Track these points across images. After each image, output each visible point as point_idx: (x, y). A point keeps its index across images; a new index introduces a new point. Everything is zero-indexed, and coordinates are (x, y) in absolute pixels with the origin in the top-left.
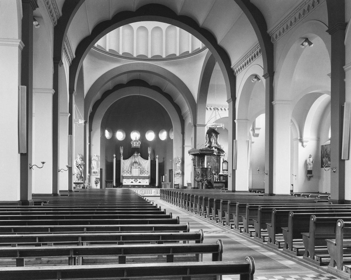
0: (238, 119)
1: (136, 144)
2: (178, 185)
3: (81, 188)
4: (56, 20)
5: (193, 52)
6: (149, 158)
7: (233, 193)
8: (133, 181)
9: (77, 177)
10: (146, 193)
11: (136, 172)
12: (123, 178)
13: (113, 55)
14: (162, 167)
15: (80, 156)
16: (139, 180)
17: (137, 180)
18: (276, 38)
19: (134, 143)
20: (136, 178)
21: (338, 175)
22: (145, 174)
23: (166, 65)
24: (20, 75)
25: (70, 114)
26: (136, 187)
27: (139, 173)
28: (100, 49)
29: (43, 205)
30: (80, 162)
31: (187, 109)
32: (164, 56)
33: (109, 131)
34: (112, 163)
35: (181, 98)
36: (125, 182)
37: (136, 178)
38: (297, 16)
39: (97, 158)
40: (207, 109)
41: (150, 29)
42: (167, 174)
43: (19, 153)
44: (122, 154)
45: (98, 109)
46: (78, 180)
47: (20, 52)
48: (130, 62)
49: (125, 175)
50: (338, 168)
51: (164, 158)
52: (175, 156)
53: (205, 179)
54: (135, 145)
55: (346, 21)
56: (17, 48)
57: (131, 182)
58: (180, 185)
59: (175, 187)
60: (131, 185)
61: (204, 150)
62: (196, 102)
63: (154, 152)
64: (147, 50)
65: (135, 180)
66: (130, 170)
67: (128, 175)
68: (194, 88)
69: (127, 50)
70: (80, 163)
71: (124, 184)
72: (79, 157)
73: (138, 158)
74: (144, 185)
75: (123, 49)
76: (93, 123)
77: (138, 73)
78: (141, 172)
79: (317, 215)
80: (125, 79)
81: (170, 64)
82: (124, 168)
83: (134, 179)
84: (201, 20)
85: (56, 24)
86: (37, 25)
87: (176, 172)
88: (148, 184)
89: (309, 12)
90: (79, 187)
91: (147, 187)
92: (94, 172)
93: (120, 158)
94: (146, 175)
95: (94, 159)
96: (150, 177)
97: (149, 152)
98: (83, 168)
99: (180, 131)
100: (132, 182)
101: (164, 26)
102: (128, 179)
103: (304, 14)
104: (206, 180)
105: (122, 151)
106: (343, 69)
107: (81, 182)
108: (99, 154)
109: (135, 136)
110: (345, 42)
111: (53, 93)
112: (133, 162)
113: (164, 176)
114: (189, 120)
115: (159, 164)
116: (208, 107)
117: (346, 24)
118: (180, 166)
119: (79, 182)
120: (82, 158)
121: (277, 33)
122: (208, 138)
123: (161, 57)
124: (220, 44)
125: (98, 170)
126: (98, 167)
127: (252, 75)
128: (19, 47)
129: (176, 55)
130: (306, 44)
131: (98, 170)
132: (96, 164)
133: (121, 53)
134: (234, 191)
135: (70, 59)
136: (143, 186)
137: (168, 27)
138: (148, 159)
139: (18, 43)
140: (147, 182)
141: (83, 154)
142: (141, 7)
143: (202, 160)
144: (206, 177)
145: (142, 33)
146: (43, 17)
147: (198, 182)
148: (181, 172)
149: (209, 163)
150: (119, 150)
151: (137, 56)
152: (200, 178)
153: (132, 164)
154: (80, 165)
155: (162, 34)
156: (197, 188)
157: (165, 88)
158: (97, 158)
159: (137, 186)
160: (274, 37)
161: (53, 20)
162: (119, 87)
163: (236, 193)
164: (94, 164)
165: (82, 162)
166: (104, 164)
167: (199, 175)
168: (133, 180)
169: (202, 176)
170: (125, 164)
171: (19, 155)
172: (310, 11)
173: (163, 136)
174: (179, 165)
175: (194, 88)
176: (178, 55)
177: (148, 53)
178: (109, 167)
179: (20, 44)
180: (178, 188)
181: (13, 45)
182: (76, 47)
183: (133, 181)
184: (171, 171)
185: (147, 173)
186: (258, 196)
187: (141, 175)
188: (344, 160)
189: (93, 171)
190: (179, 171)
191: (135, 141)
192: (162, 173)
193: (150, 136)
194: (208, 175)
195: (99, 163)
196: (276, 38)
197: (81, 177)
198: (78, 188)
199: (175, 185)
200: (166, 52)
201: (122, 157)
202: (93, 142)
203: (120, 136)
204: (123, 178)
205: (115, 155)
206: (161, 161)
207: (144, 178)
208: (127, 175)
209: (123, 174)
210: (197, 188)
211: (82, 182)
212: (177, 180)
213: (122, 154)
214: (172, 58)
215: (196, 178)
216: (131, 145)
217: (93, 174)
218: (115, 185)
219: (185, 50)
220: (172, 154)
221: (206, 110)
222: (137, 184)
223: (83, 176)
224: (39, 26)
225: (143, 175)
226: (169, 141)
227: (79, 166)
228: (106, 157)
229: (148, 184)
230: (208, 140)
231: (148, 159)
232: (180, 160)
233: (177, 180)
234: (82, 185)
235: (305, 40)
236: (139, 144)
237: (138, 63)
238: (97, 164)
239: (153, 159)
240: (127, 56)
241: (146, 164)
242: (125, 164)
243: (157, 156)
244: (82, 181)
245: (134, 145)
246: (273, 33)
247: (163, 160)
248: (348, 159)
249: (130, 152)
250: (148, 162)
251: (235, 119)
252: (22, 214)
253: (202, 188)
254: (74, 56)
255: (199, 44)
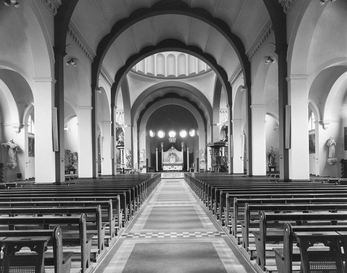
0: (234, 120)
1: (172, 140)
2: (203, 169)
3: (130, 173)
4: (92, 58)
5: (208, 70)
6: (182, 150)
7: (231, 175)
8: (171, 168)
9: (127, 165)
10: (178, 176)
11: (172, 161)
12: (164, 165)
13: (150, 77)
14: (192, 156)
15: (129, 150)
16: (175, 167)
17: (174, 167)
18: (251, 58)
19: (171, 139)
20: (172, 165)
21: (64, 162)
22: (180, 162)
23: (189, 81)
24: (54, 99)
25: (111, 122)
26: (172, 171)
27: (175, 161)
28: (140, 73)
29: (69, 185)
30: (128, 154)
31: (207, 114)
32: (187, 75)
33: (153, 131)
34: (155, 155)
35: (202, 105)
36: (165, 168)
37: (172, 165)
38: (261, 41)
39: (144, 151)
40: (221, 112)
41: (166, 56)
42: (195, 162)
43: (53, 151)
44: (162, 147)
45: (144, 117)
46: (128, 167)
47: (54, 85)
48: (161, 81)
49: (165, 163)
50: (283, 156)
51: (193, 150)
52: (200, 148)
53: (219, 165)
54: (171, 141)
55: (287, 43)
56: (50, 83)
57: (169, 168)
58: (204, 170)
59: (201, 171)
60: (169, 170)
61: (218, 143)
62: (212, 107)
63: (186, 146)
64: (175, 70)
65: (172, 167)
66: (168, 159)
67: (167, 163)
68: (211, 98)
69: (160, 72)
70: (128, 155)
71: (164, 169)
72: (127, 151)
73: (174, 151)
74: (167, 170)
75: (157, 71)
76: (140, 128)
77: (171, 89)
78: (177, 161)
79: (218, 188)
80: (161, 93)
81: (192, 80)
82: (164, 158)
83: (171, 166)
84: (203, 48)
85: (93, 61)
86: (75, 65)
87: (201, 160)
88: (181, 169)
89: (268, 37)
90: (128, 172)
91: (180, 171)
92: (141, 162)
93: (161, 150)
94: (180, 163)
95: (142, 152)
96: (183, 164)
97: (182, 146)
98: (131, 159)
99: (203, 129)
100: (170, 168)
101: (176, 54)
102: (167, 166)
103: (265, 39)
104: (220, 165)
105: (162, 146)
106: (286, 80)
107: (130, 169)
108: (145, 149)
109: (172, 134)
110: (287, 59)
111: (92, 109)
112: (171, 153)
113: (193, 163)
114: (209, 122)
115: (190, 154)
116: (221, 111)
117: (287, 45)
118: (204, 155)
119: (128, 169)
120: (130, 152)
121: (251, 54)
122: (225, 134)
123: (185, 75)
124: (219, 64)
125: (144, 159)
126: (144, 158)
127: (240, 86)
128: (52, 82)
129: (195, 73)
130: (269, 61)
131: (144, 159)
132: (143, 156)
133: (156, 75)
134: (232, 173)
135: (111, 83)
136: (177, 171)
137: (180, 55)
138: (181, 151)
139: (51, 80)
140: (180, 168)
141: (131, 149)
142: (163, 41)
143: (217, 150)
144: (220, 164)
145: (171, 59)
146: (78, 59)
147: (215, 167)
148: (205, 160)
149: (226, 153)
150: (161, 145)
151: (168, 76)
152: (215, 164)
153: (170, 155)
154: (128, 156)
155: (175, 60)
156: (214, 172)
157: (191, 98)
158: (143, 152)
159: (173, 170)
160: (250, 57)
161: (90, 59)
162: (157, 99)
163: (234, 175)
164: (141, 155)
165: (130, 154)
166: (149, 155)
167: (214, 162)
168: (170, 167)
169: (217, 162)
170: (165, 155)
171: (54, 153)
172: (269, 36)
173: (192, 133)
174: (203, 155)
175: (211, 98)
176: (197, 73)
177: (175, 73)
178: (153, 157)
179: (53, 81)
180: (203, 172)
181: (48, 81)
182: (115, 75)
183: (171, 168)
184: (198, 159)
185: (181, 161)
186: (241, 177)
187: (176, 163)
188: (288, 149)
189: (140, 160)
190: (204, 159)
191: (172, 138)
192: (191, 161)
193: (183, 134)
194: (222, 162)
195: (145, 155)
196: (251, 58)
197: (129, 165)
198: (128, 173)
199: (201, 169)
200: (189, 72)
201: (163, 150)
202: (140, 140)
203: (161, 134)
204: (164, 165)
205: (157, 149)
206: (191, 152)
207: (179, 165)
208: (166, 163)
209: (163, 162)
210: (214, 172)
211: (130, 169)
212: (202, 166)
213: (162, 147)
214: (202, 74)
215: (213, 164)
216: (169, 141)
217: (141, 163)
218: (157, 170)
219: (192, 71)
220: (198, 147)
221: (220, 113)
222: (174, 169)
223: (130, 164)
224: (76, 65)
225: (178, 163)
226: (196, 137)
227: (128, 158)
228: (151, 150)
229: (181, 169)
230: (225, 135)
231: (181, 151)
232: (204, 151)
233: (202, 166)
234: (130, 171)
235: (268, 58)
236: (175, 140)
237: (169, 81)
238: (144, 156)
239: (185, 151)
240: (160, 77)
241: (180, 155)
242: (165, 155)
243: (188, 149)
244: (130, 168)
245: (171, 141)
246: (249, 54)
247: (192, 151)
248: (290, 148)
249: (168, 146)
250: (181, 153)
251: (232, 119)
252: (57, 190)
253: (217, 172)
254: (114, 81)
255: (204, 66)
